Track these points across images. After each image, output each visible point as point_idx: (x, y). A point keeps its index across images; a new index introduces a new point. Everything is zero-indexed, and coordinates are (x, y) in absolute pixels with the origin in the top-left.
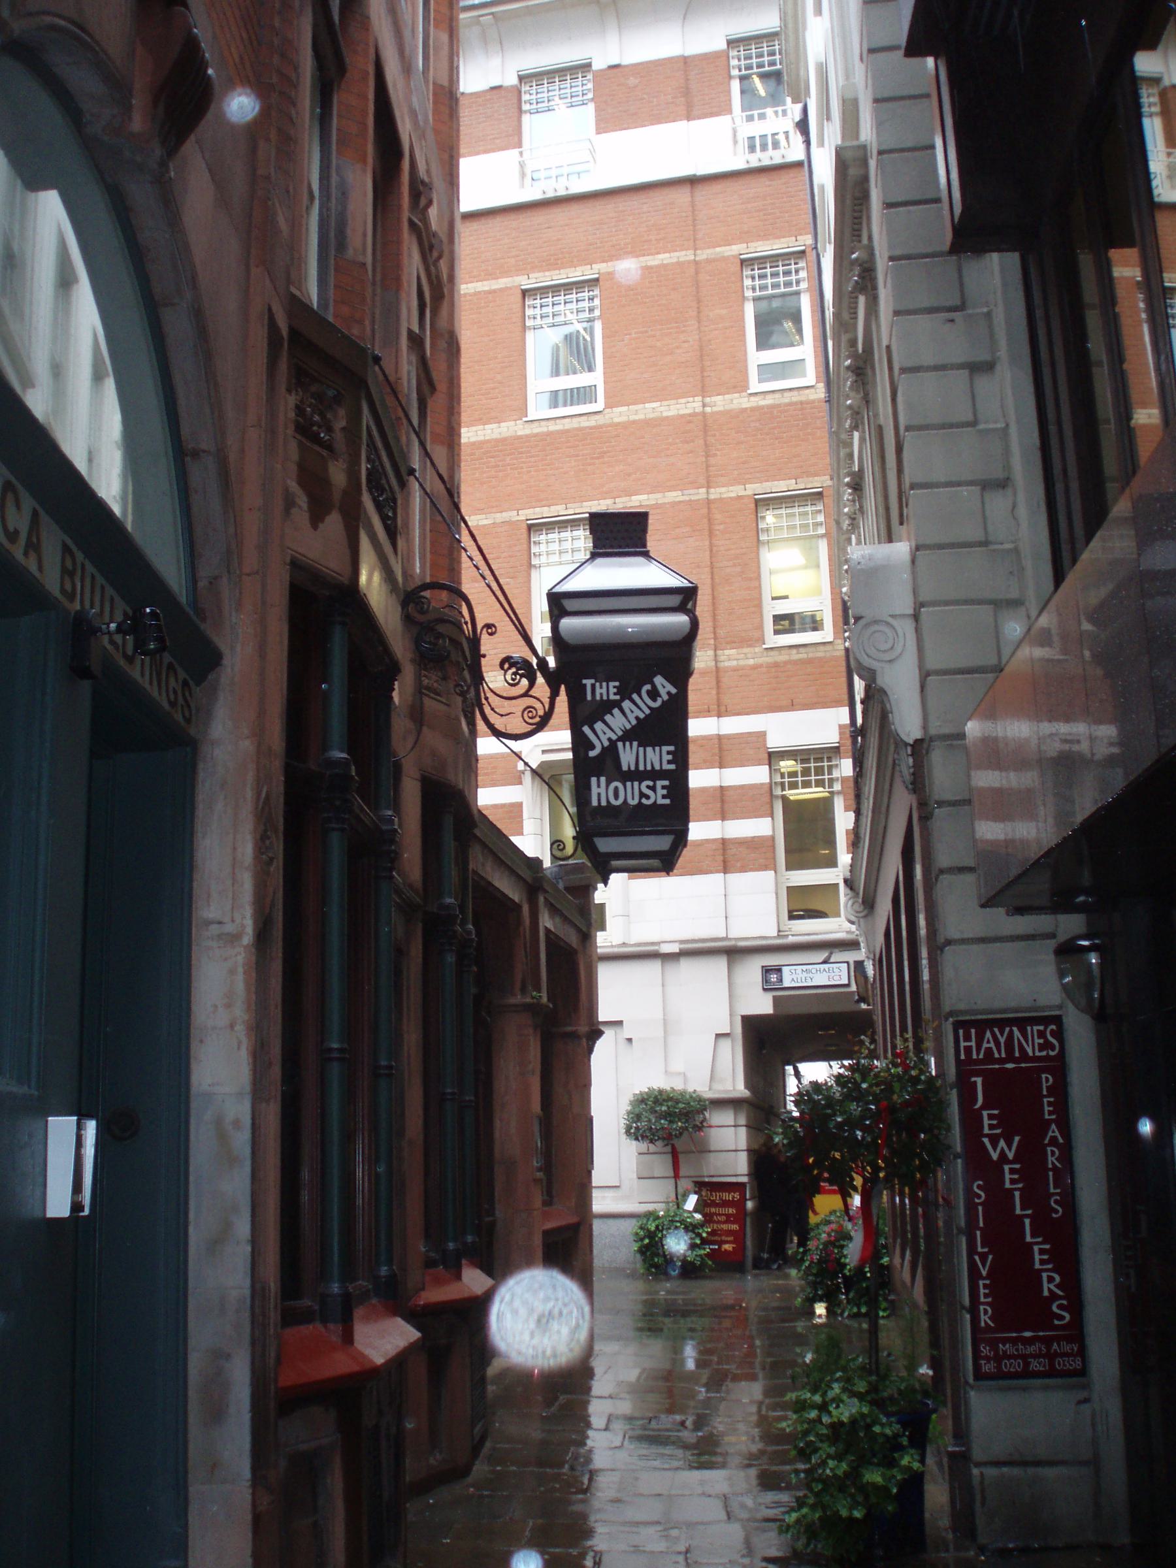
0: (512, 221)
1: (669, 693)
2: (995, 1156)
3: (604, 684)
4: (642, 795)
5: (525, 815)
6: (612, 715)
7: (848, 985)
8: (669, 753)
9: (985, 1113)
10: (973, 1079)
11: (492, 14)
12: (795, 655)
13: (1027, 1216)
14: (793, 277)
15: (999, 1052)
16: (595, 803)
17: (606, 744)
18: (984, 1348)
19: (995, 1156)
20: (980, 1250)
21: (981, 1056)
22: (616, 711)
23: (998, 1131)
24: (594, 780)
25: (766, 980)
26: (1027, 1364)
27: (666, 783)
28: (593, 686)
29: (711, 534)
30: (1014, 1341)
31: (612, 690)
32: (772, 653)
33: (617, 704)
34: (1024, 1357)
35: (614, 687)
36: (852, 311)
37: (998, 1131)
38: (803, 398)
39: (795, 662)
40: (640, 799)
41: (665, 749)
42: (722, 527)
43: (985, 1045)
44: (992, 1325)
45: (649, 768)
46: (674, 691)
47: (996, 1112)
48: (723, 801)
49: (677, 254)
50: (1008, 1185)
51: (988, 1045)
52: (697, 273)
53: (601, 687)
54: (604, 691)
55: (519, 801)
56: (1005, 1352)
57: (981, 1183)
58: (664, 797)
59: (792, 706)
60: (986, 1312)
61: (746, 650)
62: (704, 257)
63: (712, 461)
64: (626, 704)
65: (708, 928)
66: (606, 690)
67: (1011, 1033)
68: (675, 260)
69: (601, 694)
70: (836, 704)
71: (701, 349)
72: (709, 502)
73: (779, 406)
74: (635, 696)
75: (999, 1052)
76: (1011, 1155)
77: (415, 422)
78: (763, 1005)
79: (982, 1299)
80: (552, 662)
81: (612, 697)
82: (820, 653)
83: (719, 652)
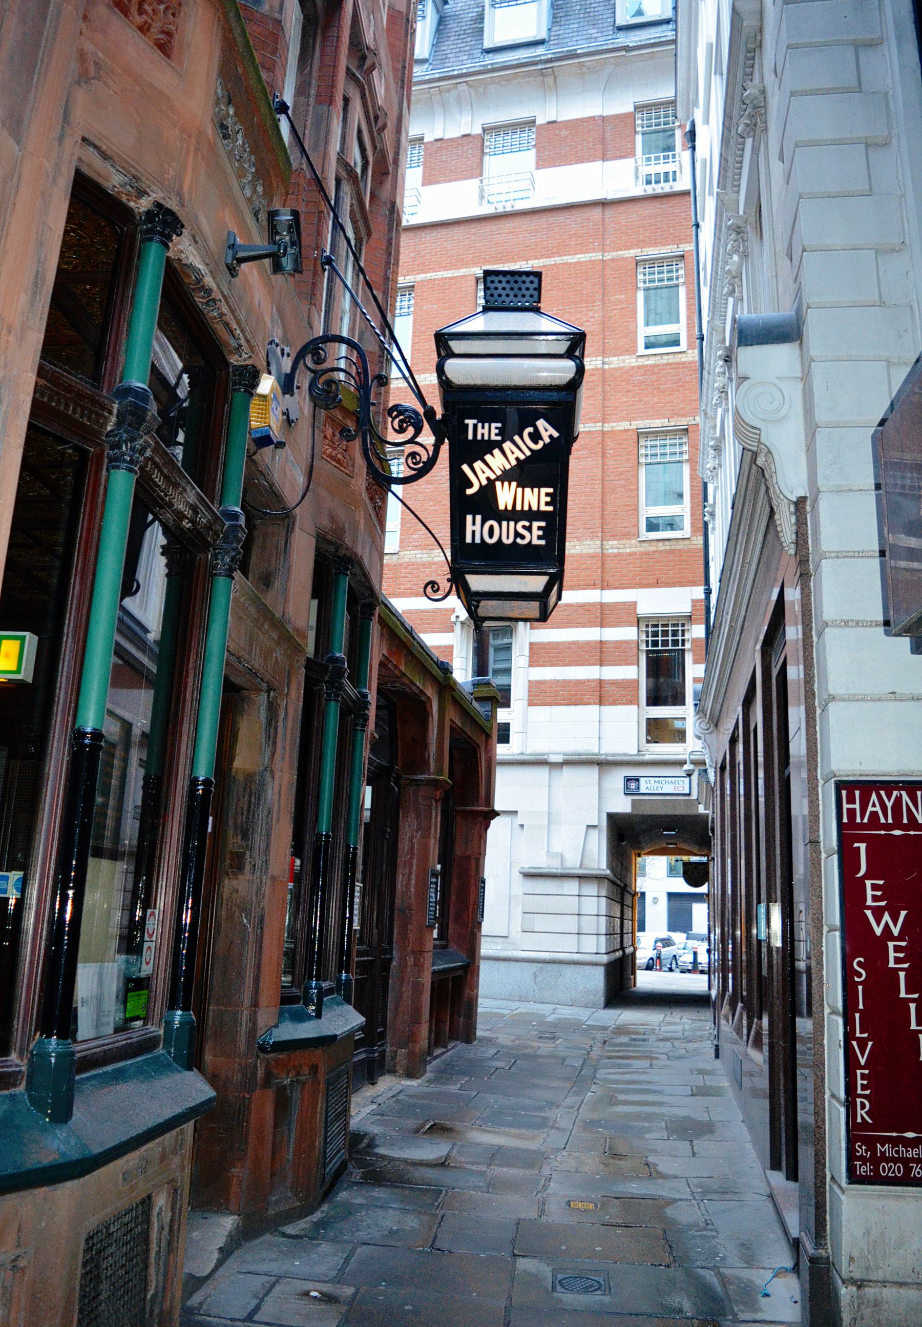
0: (473, 229)
1: (551, 437)
2: (878, 931)
3: (486, 425)
4: (517, 535)
5: (455, 655)
6: (492, 455)
7: (689, 795)
8: (547, 495)
9: (868, 883)
10: (856, 845)
11: (466, 82)
12: (661, 547)
13: (913, 1000)
14: (674, 274)
15: (886, 818)
16: (469, 540)
17: (484, 482)
18: (860, 1147)
19: (878, 931)
20: (858, 1035)
21: (865, 821)
22: (496, 452)
23: (883, 903)
24: (469, 518)
25: (627, 787)
26: (908, 1170)
27: (543, 524)
28: (475, 426)
29: (604, 456)
30: (894, 1142)
31: (494, 431)
32: (644, 545)
33: (499, 445)
34: (906, 1162)
35: (496, 428)
36: (740, 146)
37: (883, 903)
38: (677, 360)
39: (661, 552)
40: (515, 538)
41: (544, 490)
42: (612, 451)
43: (870, 809)
44: (870, 1121)
45: (526, 508)
46: (556, 434)
47: (881, 882)
48: (601, 652)
49: (590, 255)
50: (892, 964)
51: (874, 809)
52: (604, 268)
53: (483, 428)
54: (486, 431)
55: (451, 643)
56: (883, 1153)
57: (862, 960)
58: (539, 538)
59: (657, 584)
60: (863, 1106)
61: (624, 542)
62: (610, 257)
63: (608, 404)
64: (507, 446)
65: (588, 746)
66: (489, 431)
67: (899, 800)
68: (588, 259)
69: (483, 435)
70: (694, 583)
71: (604, 322)
72: (603, 433)
73: (659, 365)
74: (517, 438)
75: (886, 818)
76: (896, 931)
77: (332, 203)
78: (623, 805)
79: (859, 1092)
80: (439, 414)
81: (493, 437)
82: (681, 546)
83: (605, 543)
